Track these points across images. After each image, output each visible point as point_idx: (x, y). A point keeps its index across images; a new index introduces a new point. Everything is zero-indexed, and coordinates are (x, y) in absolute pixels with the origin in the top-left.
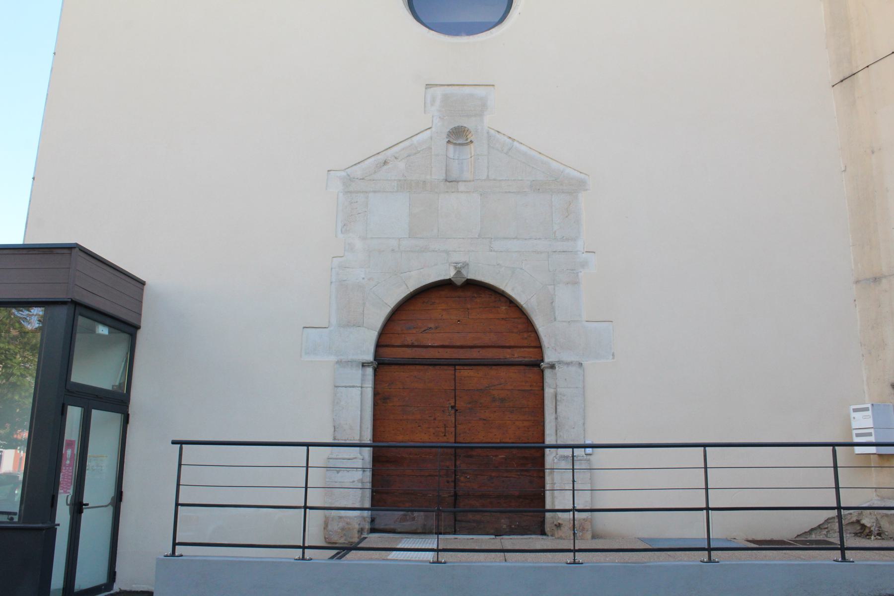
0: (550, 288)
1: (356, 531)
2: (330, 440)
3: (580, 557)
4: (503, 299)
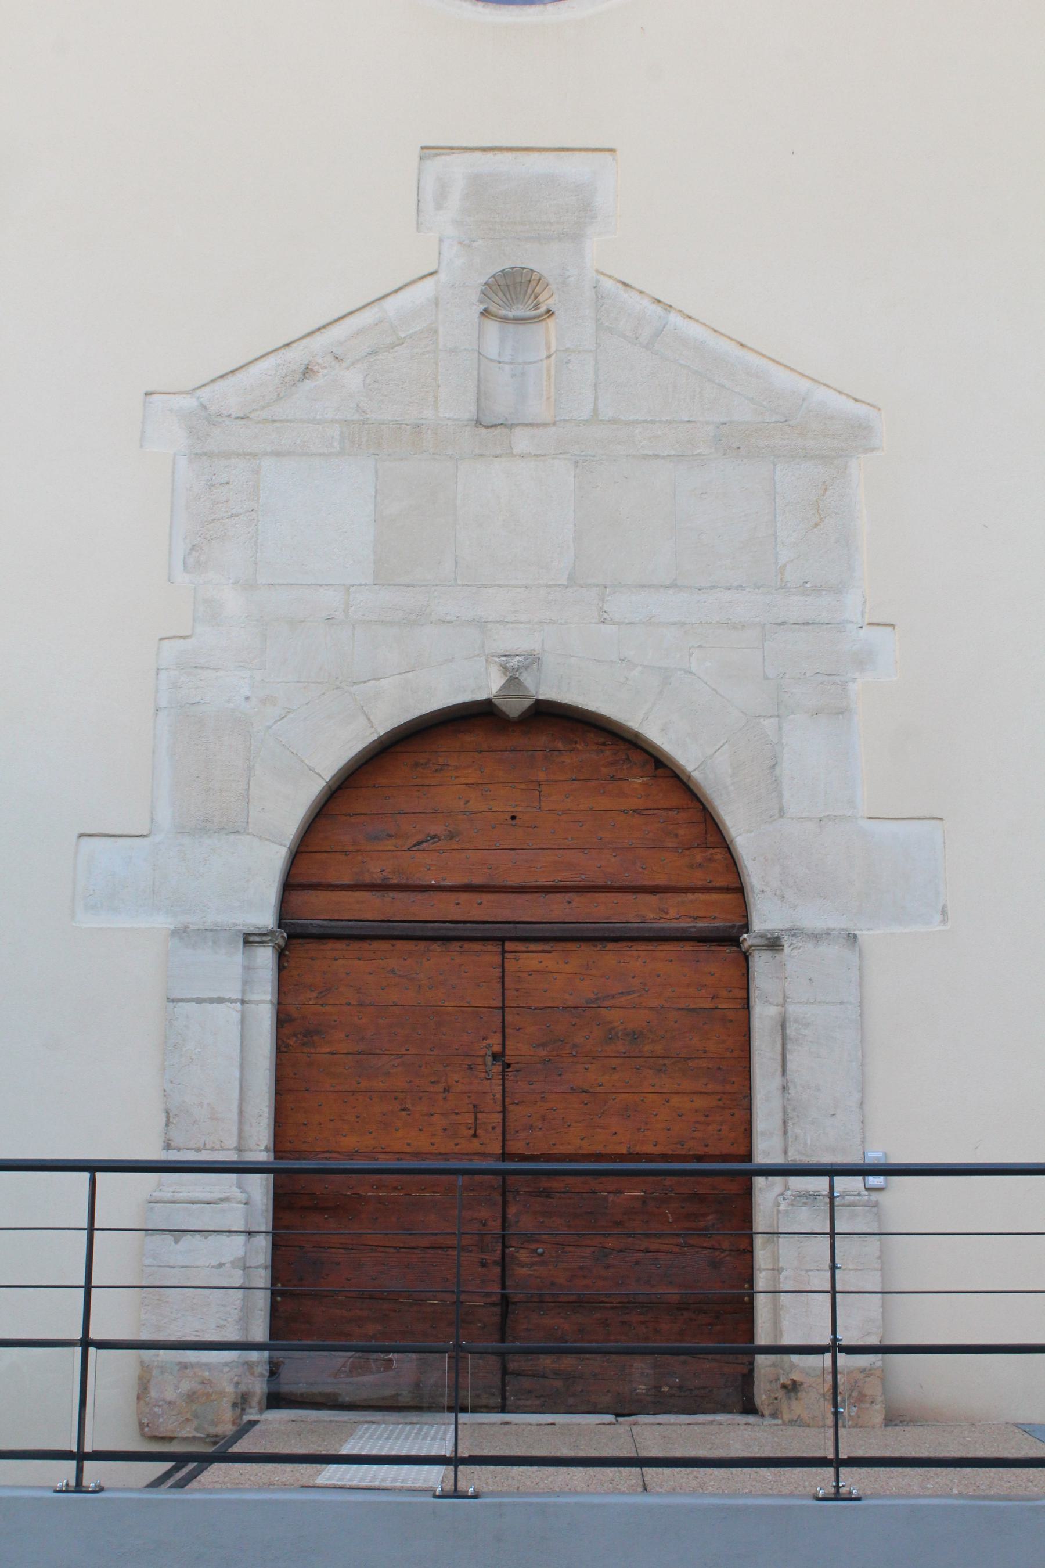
0: (769, 724)
1: (226, 1405)
2: (154, 1153)
3: (852, 1479)
4: (637, 757)
